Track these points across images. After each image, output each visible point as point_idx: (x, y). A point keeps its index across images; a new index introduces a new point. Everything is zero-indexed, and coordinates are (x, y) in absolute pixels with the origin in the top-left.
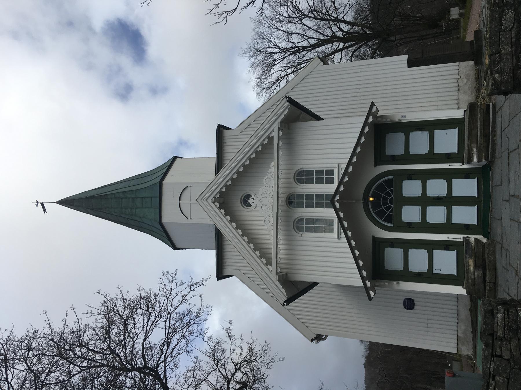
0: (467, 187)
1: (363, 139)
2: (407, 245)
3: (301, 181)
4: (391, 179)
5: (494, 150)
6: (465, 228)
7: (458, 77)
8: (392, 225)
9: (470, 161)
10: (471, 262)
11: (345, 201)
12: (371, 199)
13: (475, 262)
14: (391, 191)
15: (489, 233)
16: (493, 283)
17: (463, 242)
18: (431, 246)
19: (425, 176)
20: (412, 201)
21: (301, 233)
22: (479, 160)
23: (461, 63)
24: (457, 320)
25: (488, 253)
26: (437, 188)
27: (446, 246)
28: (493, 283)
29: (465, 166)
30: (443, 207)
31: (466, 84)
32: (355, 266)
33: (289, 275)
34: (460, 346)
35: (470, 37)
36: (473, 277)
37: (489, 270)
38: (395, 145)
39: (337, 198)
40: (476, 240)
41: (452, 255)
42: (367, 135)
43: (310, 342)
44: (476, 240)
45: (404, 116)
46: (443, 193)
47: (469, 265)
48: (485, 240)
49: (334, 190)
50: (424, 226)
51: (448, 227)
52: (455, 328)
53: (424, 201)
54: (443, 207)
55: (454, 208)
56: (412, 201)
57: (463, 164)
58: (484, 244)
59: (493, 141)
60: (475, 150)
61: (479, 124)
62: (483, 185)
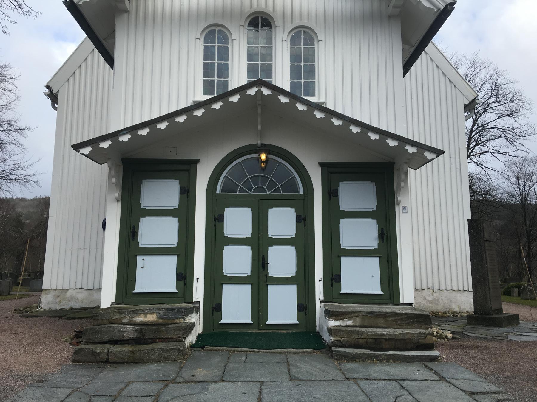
0: (283, 307)
1: (373, 137)
2: (185, 215)
3: (294, 40)
4: (297, 191)
5: (352, 358)
6: (214, 306)
7: (436, 288)
8: (218, 192)
9: (330, 314)
10: (151, 318)
11: (259, 111)
12: (263, 157)
13: (152, 324)
14: (278, 190)
15: (203, 348)
16: (108, 358)
17: (192, 303)
18: (183, 252)
19: (303, 242)
20: (260, 223)
21: (202, 39)
22: (331, 331)
23: (471, 295)
24: (89, 288)
25: (163, 349)
26: (282, 261)
27: (184, 276)
28: (108, 358)
29: (319, 306)
30: (254, 267)
31: (425, 299)
32: (137, 122)
33: (126, 15)
34: (54, 293)
35: (508, 309)
36: (125, 321)
37: (132, 352)
38: (355, 196)
39: (266, 92)
40: (191, 326)
41: (169, 285)
42: (381, 143)
43: (45, 84)
44: (191, 326)
45: (405, 210)
46: (273, 271)
47: (146, 314)
48: (192, 339)
49: (279, 85)
50: (217, 242)
51: (216, 279)
52: (79, 286)
53: (260, 242)
54: (254, 267)
55: (247, 289)
56: (260, 223)
57: (322, 302)
58: (181, 340)
59: (370, 357)
60: (350, 323)
61: (398, 331)
62: (285, 334)
